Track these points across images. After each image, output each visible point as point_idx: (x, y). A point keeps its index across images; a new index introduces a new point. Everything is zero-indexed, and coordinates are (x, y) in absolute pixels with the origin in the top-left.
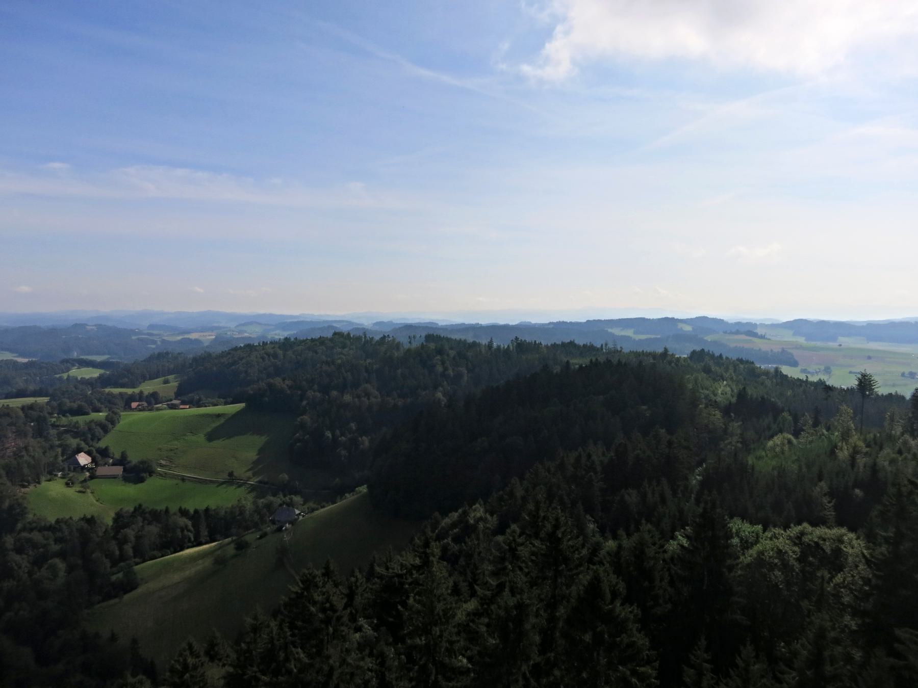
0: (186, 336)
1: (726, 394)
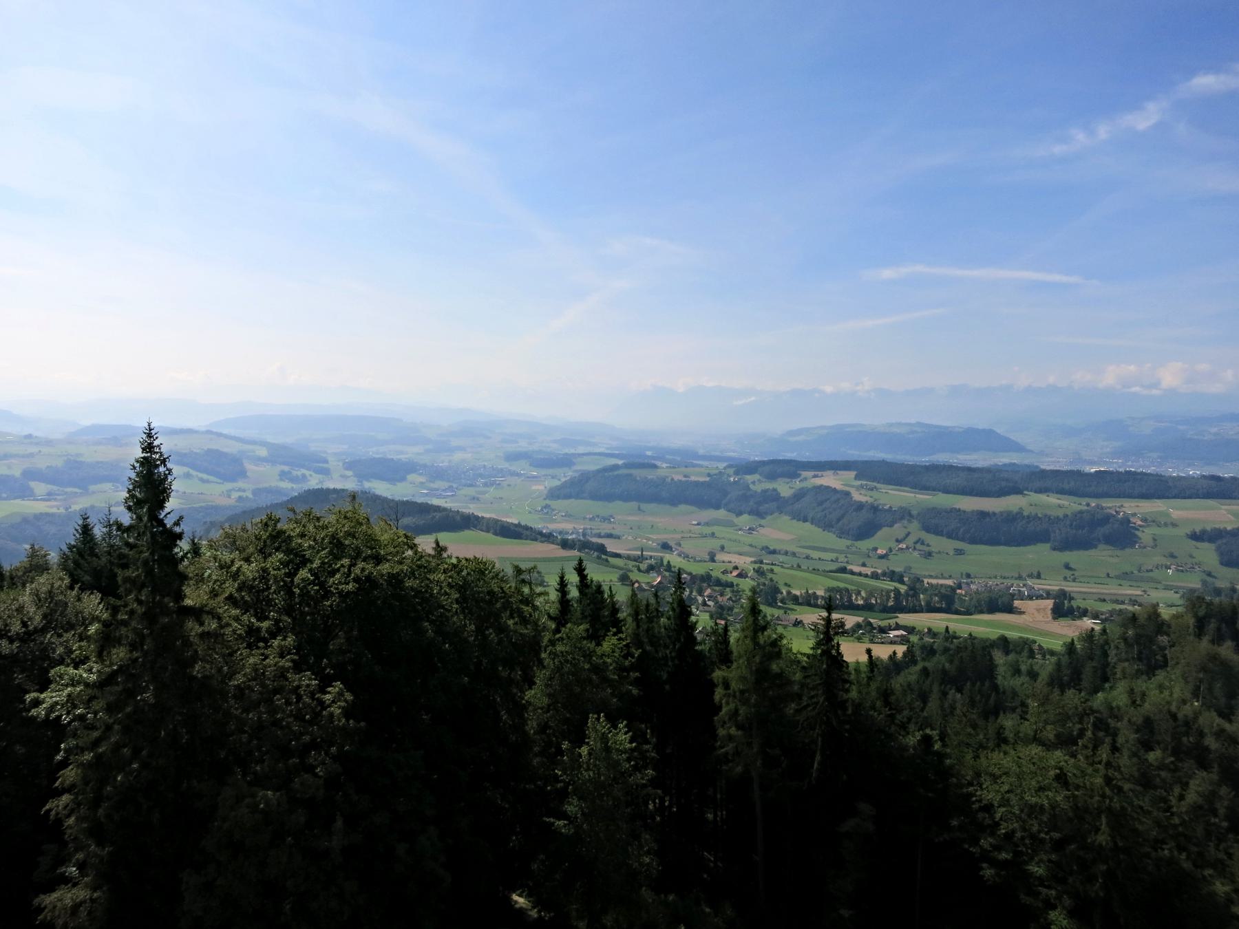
1: (908, 520)
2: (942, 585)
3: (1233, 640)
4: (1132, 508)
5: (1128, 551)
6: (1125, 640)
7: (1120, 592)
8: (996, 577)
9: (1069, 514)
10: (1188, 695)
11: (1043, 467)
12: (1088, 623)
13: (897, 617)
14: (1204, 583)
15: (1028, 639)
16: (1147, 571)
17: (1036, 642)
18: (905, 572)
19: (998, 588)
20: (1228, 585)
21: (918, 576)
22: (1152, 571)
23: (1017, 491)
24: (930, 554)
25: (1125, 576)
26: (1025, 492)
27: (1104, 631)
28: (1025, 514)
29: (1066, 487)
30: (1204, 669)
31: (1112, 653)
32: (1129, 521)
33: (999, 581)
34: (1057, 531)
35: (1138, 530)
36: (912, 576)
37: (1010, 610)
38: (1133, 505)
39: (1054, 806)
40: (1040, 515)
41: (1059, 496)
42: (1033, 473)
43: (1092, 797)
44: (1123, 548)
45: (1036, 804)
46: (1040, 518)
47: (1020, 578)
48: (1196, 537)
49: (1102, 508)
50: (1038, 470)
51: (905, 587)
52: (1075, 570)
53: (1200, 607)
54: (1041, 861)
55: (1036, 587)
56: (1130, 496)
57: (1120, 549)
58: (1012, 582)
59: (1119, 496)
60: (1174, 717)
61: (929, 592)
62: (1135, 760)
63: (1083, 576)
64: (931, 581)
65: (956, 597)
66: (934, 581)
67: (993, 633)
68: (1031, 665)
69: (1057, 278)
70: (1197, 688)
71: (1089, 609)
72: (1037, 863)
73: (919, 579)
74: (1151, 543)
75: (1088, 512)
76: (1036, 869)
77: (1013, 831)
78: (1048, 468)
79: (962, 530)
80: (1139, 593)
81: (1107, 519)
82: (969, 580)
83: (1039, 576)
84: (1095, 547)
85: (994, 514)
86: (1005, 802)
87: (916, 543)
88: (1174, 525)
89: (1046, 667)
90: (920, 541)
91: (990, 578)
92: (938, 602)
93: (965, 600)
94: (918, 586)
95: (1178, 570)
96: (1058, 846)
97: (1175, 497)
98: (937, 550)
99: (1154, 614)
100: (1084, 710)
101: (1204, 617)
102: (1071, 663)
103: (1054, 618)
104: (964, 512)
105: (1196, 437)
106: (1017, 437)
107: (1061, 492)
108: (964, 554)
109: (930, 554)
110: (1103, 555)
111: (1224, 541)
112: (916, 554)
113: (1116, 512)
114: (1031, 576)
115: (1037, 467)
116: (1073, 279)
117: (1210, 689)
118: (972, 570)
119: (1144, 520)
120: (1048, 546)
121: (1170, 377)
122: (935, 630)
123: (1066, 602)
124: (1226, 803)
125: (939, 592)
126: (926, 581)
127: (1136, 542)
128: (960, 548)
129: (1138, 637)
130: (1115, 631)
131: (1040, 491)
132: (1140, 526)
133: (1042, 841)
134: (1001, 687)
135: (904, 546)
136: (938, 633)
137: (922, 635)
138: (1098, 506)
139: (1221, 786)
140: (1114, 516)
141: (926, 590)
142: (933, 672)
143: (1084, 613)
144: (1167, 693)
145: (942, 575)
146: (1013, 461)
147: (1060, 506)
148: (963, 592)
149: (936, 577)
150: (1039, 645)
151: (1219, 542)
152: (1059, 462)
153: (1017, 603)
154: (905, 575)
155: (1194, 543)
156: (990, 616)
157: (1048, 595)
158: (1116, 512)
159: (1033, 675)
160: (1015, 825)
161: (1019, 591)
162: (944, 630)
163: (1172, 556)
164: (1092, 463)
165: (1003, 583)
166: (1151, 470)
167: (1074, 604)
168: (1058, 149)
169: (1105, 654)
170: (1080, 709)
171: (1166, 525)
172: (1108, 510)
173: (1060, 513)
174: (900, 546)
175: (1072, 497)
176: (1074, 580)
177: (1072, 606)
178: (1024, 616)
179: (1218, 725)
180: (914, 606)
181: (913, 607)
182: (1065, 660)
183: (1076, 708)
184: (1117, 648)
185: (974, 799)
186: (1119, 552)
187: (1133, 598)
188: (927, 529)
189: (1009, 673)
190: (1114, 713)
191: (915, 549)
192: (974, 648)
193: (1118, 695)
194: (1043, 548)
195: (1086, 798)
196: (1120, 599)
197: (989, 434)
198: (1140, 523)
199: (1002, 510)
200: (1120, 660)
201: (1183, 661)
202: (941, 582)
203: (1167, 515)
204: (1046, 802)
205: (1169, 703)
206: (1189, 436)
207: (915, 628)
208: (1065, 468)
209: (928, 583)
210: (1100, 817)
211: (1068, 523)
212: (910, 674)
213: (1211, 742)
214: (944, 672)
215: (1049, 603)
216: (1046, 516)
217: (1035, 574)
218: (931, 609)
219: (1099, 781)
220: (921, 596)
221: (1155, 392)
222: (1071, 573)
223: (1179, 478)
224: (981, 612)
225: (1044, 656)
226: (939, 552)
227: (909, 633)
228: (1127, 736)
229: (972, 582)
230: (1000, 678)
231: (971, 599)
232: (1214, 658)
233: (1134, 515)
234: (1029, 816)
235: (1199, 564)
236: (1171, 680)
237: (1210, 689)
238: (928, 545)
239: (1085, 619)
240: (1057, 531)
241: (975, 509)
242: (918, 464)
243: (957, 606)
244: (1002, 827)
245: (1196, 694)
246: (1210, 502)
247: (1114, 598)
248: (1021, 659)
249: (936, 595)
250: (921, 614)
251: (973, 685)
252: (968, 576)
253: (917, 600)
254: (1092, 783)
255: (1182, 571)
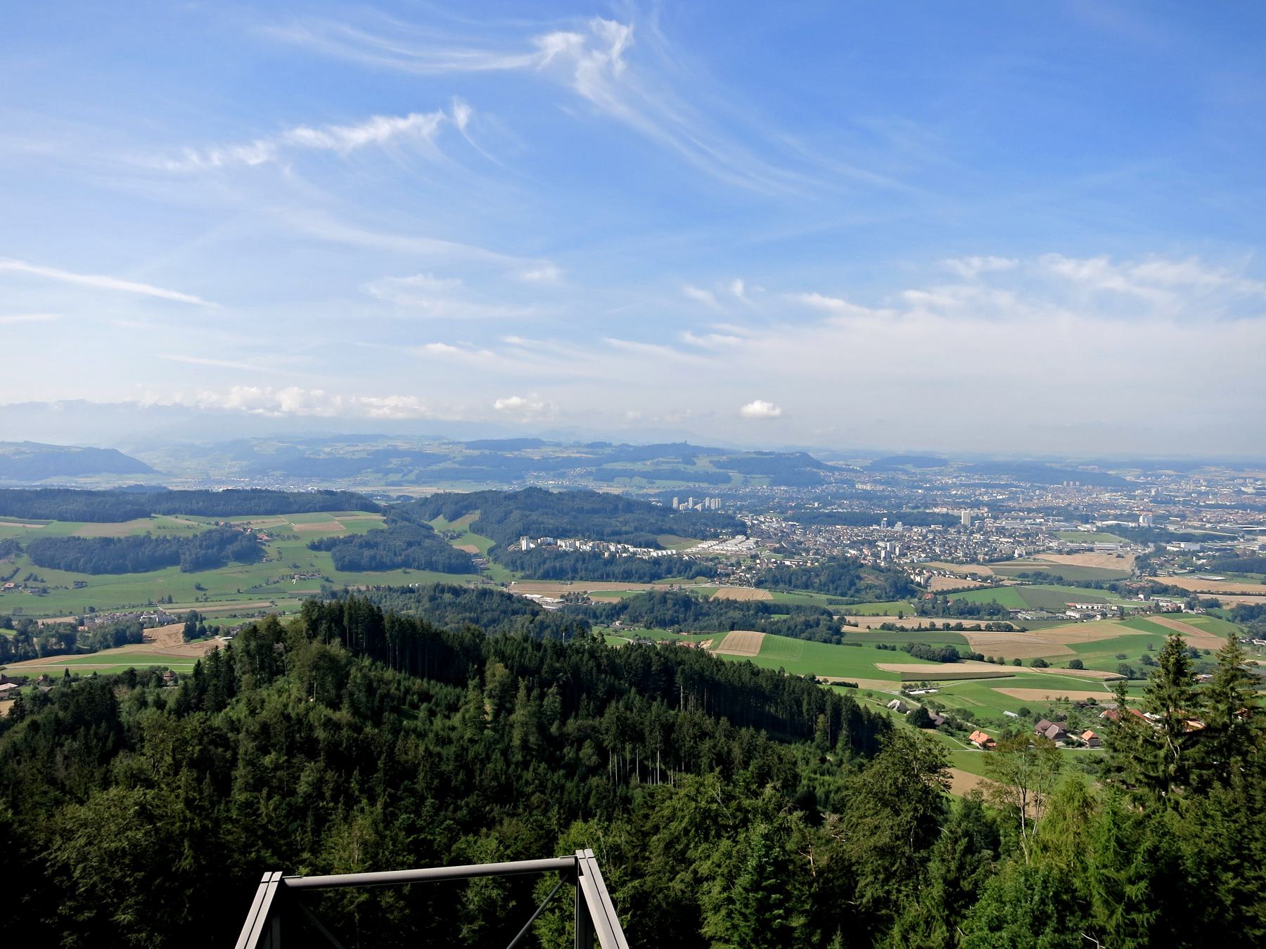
0: (686, 640)
2: (60, 624)
3: (340, 637)
4: (260, 524)
5: (256, 565)
6: (248, 653)
7: (250, 606)
8: (123, 607)
9: (198, 534)
10: (304, 695)
11: (170, 488)
12: (221, 641)
13: (4, 669)
14: (323, 587)
15: (159, 667)
16: (275, 583)
17: (167, 669)
18: (14, 615)
19: (126, 618)
20: (343, 587)
21: (30, 618)
22: (278, 582)
23: (142, 513)
24: (45, 591)
25: (255, 590)
26: (153, 515)
27: (229, 647)
28: (154, 537)
29: (195, 507)
30: (316, 667)
31: (237, 667)
32: (256, 537)
33: (127, 611)
34: (187, 552)
35: (265, 545)
36: (23, 618)
37: (139, 639)
38: (259, 521)
39: (134, 845)
40: (168, 538)
41: (188, 517)
42: (160, 495)
43: (173, 824)
44: (252, 563)
45: (117, 850)
46: (168, 541)
47: (150, 604)
48: (315, 547)
49: (231, 526)
50: (165, 491)
51: (14, 633)
52: (206, 590)
53: (314, 610)
54: (128, 907)
55: (168, 612)
56: (256, 513)
57: (250, 564)
58: (141, 610)
59: (247, 514)
60: (287, 717)
61: (44, 634)
62: (249, 768)
63: (216, 595)
64: (45, 621)
65: (78, 634)
66: (50, 621)
67: (118, 668)
68: (158, 695)
69: (176, 295)
70: (311, 686)
71: (221, 626)
72: (123, 910)
73: (31, 621)
74: (277, 556)
75: (216, 531)
76: (123, 917)
77: (94, 885)
78: (176, 489)
79: (82, 560)
80: (268, 604)
81: (235, 536)
82: (93, 614)
83: (170, 601)
84: (225, 564)
85: (120, 540)
86: (84, 858)
87: (27, 579)
88: (296, 538)
89: (172, 693)
90: (32, 577)
91: (118, 609)
92: (55, 644)
93: (88, 637)
94: (30, 628)
95: (301, 579)
96: (143, 885)
97: (297, 512)
98: (53, 586)
99: (274, 625)
100: (203, 730)
101: (317, 620)
102: (198, 684)
103: (186, 642)
104: (85, 540)
105: (312, 456)
106: (143, 457)
107: (192, 512)
108: (86, 586)
109: (45, 591)
110: (233, 572)
111: (338, 549)
112: (27, 592)
113: (244, 529)
114: (162, 601)
115: (165, 488)
116: (194, 299)
117: (322, 686)
118: (94, 602)
119: (271, 535)
120: (177, 569)
121: (289, 400)
122: (52, 676)
123: (197, 623)
124: (331, 785)
125: (57, 632)
126: (40, 622)
127: (263, 556)
128: (80, 581)
129: (260, 647)
130: (238, 645)
131: (168, 513)
132: (266, 541)
133: (127, 884)
134: (125, 724)
135: (12, 585)
136: (56, 679)
137: (36, 684)
138: (226, 524)
139: (327, 771)
140: (242, 533)
141: (41, 632)
142: (44, 724)
143: (216, 632)
144: (285, 696)
145: (61, 612)
146: (139, 483)
147: (188, 527)
148: (86, 628)
149: (55, 616)
150: (171, 672)
151: (334, 550)
152: (188, 482)
153: (146, 632)
154: (13, 618)
155: (314, 552)
156: (115, 650)
157: (180, 618)
158: (244, 529)
159: (160, 705)
160: (95, 879)
161: (150, 618)
162: (63, 675)
163: (295, 566)
164: (220, 482)
165: (132, 613)
166: (275, 488)
167: (206, 624)
168: (171, 165)
169: (231, 669)
170: (200, 730)
171: (289, 538)
172: (236, 528)
173: (190, 535)
174: (7, 585)
175: (200, 518)
176: (206, 601)
177: (204, 627)
178: (154, 644)
179: (325, 716)
180: (26, 653)
181: (24, 653)
182: (191, 682)
183: (196, 730)
184: (241, 661)
185: (48, 864)
186: (248, 568)
187: (262, 610)
188: (40, 562)
189: (135, 708)
190: (234, 726)
191: (26, 587)
192: (91, 688)
193: (237, 710)
194: (174, 570)
195: (169, 827)
196: (250, 613)
197: (113, 453)
198: (266, 538)
199: (127, 535)
200: (244, 673)
201: (299, 663)
202: (59, 620)
203: (289, 529)
204: (125, 844)
205: (286, 706)
206: (307, 456)
207: (28, 678)
208: (194, 489)
209: (43, 624)
210: (183, 843)
211: (197, 543)
212: (16, 732)
213: (320, 734)
214: (58, 721)
215: (181, 627)
216: (174, 538)
217: (166, 598)
218: (47, 653)
219: (180, 806)
220: (35, 640)
221: (276, 414)
222: (202, 593)
223: (300, 494)
224: (108, 647)
225: (176, 681)
226: (57, 588)
227: (20, 685)
228: (246, 745)
229: (96, 616)
230: (124, 714)
231: (95, 636)
232: (324, 656)
233: (261, 530)
234: (111, 864)
235: (319, 571)
236: (289, 683)
237: (322, 686)
238: (42, 581)
239: (217, 637)
240: (187, 552)
241: (98, 536)
242: (27, 489)
243: (79, 644)
244: (81, 885)
245: (310, 692)
246: (325, 514)
247: (245, 612)
248: (147, 690)
249: (53, 636)
250: (36, 661)
251: (88, 729)
252: (92, 610)
253: (29, 645)
254: (173, 811)
255: (305, 579)
